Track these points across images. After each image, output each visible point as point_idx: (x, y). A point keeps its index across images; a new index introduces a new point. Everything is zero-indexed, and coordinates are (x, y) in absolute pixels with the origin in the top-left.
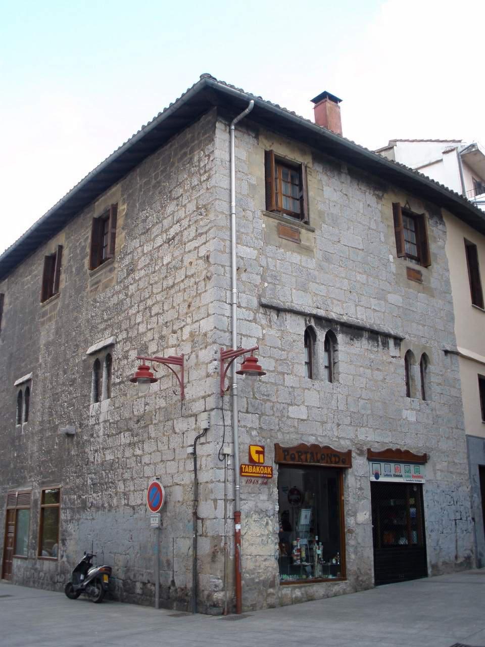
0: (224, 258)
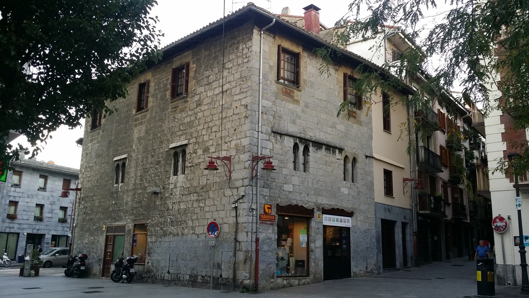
0: (256, 106)
